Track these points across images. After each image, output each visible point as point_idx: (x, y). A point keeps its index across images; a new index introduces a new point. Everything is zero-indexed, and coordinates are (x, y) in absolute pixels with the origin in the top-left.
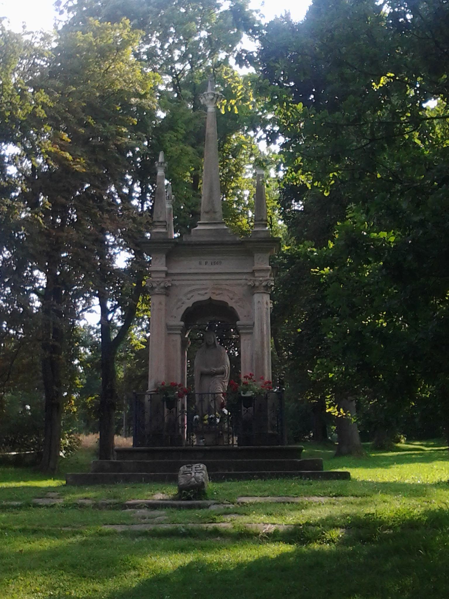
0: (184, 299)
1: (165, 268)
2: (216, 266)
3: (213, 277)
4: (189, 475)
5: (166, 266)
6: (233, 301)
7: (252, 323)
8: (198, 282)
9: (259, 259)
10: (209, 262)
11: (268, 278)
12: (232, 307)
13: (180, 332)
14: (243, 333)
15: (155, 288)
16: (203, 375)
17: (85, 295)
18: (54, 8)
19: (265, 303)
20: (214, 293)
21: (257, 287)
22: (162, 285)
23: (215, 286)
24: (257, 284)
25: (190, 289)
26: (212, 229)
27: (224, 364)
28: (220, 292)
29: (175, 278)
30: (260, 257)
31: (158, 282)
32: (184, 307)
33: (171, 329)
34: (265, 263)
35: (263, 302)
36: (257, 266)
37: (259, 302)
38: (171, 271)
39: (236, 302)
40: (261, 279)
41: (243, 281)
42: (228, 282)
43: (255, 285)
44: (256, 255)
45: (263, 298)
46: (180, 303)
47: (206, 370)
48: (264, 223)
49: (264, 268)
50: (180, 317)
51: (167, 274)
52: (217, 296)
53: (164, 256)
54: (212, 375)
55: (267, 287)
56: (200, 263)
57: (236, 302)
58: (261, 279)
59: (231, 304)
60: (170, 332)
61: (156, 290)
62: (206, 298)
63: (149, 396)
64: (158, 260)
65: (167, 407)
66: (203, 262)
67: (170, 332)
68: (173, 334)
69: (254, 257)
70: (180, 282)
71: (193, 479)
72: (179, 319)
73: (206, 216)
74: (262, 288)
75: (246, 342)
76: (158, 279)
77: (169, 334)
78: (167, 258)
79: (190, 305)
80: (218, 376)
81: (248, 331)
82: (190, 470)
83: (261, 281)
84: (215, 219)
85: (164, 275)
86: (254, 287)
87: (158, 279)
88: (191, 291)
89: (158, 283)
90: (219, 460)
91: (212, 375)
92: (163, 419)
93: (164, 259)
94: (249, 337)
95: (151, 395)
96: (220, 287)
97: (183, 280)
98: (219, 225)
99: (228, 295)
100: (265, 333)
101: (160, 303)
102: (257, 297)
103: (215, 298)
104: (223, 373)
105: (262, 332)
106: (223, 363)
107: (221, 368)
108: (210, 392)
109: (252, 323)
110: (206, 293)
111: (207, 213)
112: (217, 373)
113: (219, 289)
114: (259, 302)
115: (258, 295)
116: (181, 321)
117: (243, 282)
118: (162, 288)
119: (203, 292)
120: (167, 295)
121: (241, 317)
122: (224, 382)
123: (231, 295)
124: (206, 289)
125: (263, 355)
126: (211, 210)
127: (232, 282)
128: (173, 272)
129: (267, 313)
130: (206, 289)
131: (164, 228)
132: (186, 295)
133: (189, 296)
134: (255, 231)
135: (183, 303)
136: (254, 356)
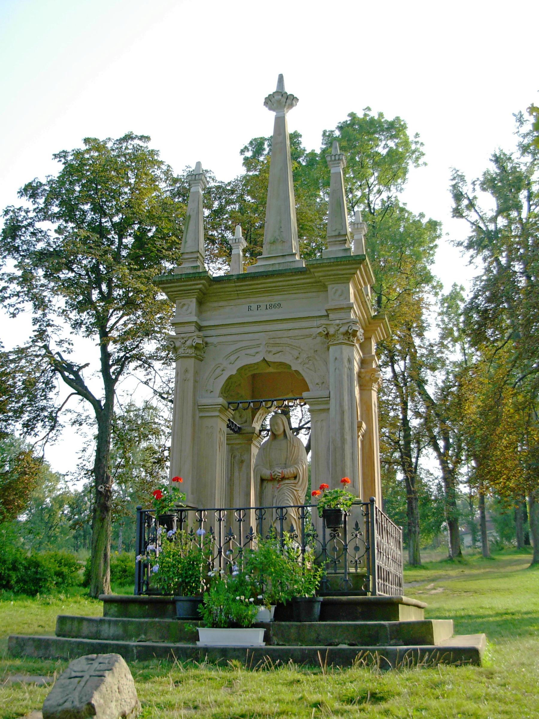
1: (195, 319)
2: (273, 310)
3: (269, 327)
8: (246, 335)
15: (180, 348)
20: (270, 352)
21: (334, 335)
22: (189, 343)
23: (271, 341)
24: (332, 331)
25: (233, 348)
28: (279, 349)
30: (337, 290)
31: (183, 338)
33: (201, 410)
36: (331, 304)
37: (336, 359)
40: (338, 322)
42: (291, 333)
45: (342, 353)
46: (218, 371)
49: (342, 306)
50: (218, 391)
51: (200, 328)
52: (277, 355)
58: (338, 322)
60: (202, 414)
62: (258, 359)
64: (185, 307)
67: (202, 414)
68: (497, 590)
70: (222, 339)
74: (341, 337)
78: (200, 303)
80: (287, 481)
81: (322, 407)
83: (338, 325)
85: (192, 328)
87: (182, 335)
88: (236, 351)
96: (278, 341)
97: (257, 284)
103: (270, 358)
105: (341, 406)
109: (326, 394)
113: (276, 345)
114: (336, 359)
118: (192, 347)
119: (253, 351)
123: (295, 353)
124: (258, 346)
130: (258, 346)
133: (233, 358)
136: (331, 447)
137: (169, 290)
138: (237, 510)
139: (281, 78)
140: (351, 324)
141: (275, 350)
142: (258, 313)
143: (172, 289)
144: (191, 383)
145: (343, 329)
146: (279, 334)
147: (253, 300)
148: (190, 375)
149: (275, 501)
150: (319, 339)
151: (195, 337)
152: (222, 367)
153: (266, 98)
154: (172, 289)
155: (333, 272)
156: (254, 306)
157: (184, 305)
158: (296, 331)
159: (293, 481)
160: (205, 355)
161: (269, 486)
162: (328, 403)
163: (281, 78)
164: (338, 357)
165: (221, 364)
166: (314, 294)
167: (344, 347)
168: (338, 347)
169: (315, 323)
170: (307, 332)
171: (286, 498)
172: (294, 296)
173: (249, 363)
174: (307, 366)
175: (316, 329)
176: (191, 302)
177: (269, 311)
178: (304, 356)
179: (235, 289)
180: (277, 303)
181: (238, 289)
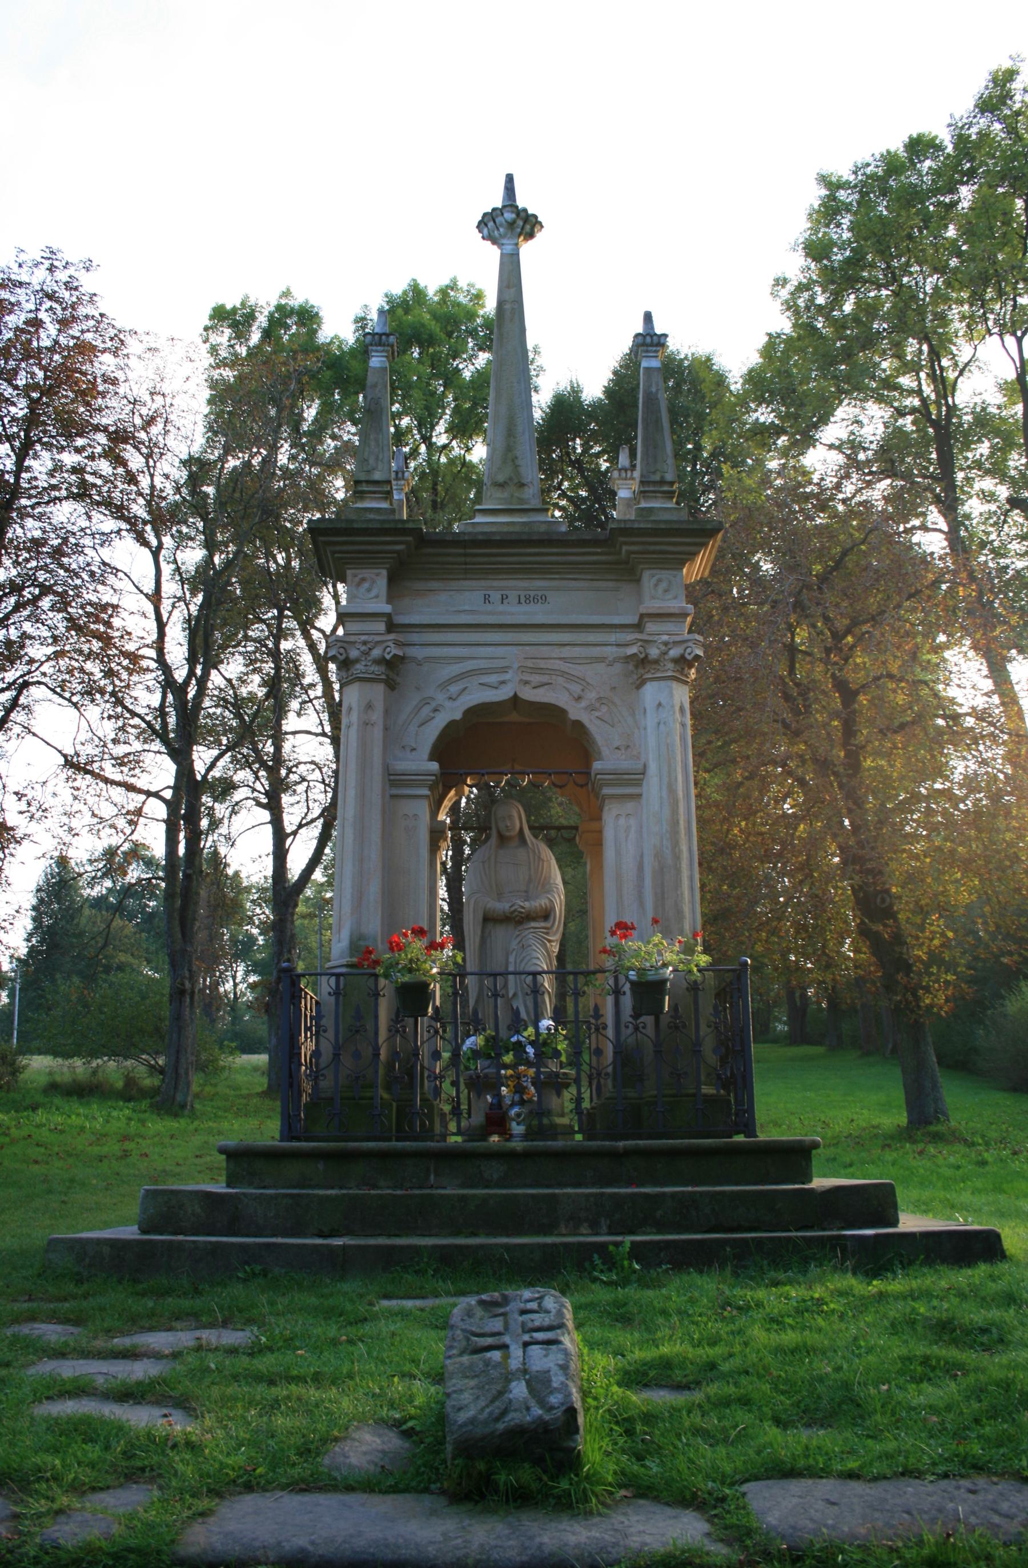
0: (440, 697)
1: (387, 609)
4: (496, 1355)
5: (388, 602)
6: (583, 704)
7: (641, 766)
9: (656, 585)
10: (513, 595)
11: (686, 636)
12: (578, 725)
13: (426, 792)
14: (613, 797)
15: (357, 661)
16: (489, 919)
17: (12, 481)
18: (201, 331)
19: (677, 708)
20: (527, 683)
21: (656, 662)
22: (376, 653)
23: (529, 663)
24: (654, 652)
26: (356, 1141)
27: (549, 891)
28: (545, 679)
29: (415, 638)
30: (660, 580)
31: (365, 643)
32: (440, 721)
33: (393, 784)
34: (675, 598)
35: (673, 706)
37: (660, 705)
38: (399, 619)
39: (591, 708)
41: (609, 649)
42: (566, 652)
43: (646, 656)
44: (646, 575)
46: (426, 711)
47: (502, 906)
48: (666, 488)
49: (672, 611)
51: (392, 627)
52: (541, 691)
53: (384, 572)
54: (518, 919)
55: (683, 662)
56: (487, 599)
57: (591, 708)
58: (665, 638)
59: (576, 712)
60: (395, 791)
61: (360, 666)
62: (503, 694)
63: (333, 980)
64: (366, 585)
65: (474, 517)
66: (495, 596)
67: (395, 791)
69: (638, 581)
71: (519, 1390)
72: (426, 756)
73: (499, 494)
74: (670, 666)
75: (622, 821)
76: (363, 638)
77: (392, 796)
78: (391, 580)
79: (458, 716)
80: (533, 924)
82: (497, 1325)
83: (666, 644)
84: (521, 501)
85: (381, 627)
86: (643, 662)
87: (363, 638)
89: (363, 648)
90: (557, 1191)
91: (518, 919)
92: (377, 1055)
93: (382, 583)
94: (630, 806)
95: (338, 976)
96: (542, 664)
97: (449, 555)
98: (531, 514)
99: (567, 690)
100: (680, 794)
101: (369, 706)
102: (650, 691)
103: (528, 694)
104: (546, 915)
105: (672, 790)
106: (546, 886)
107: (542, 902)
108: (511, 969)
110: (503, 682)
111: (501, 485)
112: (529, 917)
114: (660, 705)
115: (655, 684)
116: (431, 758)
117: (610, 652)
119: (493, 679)
120: (391, 685)
121: (605, 751)
122: (550, 941)
123: (576, 688)
124: (504, 670)
125: (677, 858)
126: (511, 479)
127: (577, 652)
128: (407, 622)
129: (683, 739)
130: (504, 670)
131: (386, 499)
132: (444, 685)
133: (454, 689)
134: (643, 509)
135: (436, 710)
137: (338, 548)
138: (490, 975)
139: (510, 179)
140: (690, 644)
141: (536, 679)
142: (501, 608)
143: (345, 548)
144: (378, 733)
145: (675, 652)
146: (545, 651)
147: (496, 583)
148: (377, 716)
149: (512, 959)
150: (618, 667)
151: (390, 644)
152: (433, 704)
153: (485, 215)
154: (345, 548)
155: (658, 548)
156: (495, 596)
157: (363, 580)
158: (577, 649)
159: (543, 924)
160: (398, 680)
161: (500, 934)
162: (638, 783)
163: (510, 179)
164: (663, 702)
165: (433, 699)
166: (611, 584)
167: (675, 685)
168: (663, 683)
169: (613, 637)
170: (596, 651)
171: (535, 954)
172: (573, 584)
173: (487, 700)
174: (597, 714)
175: (614, 649)
176: (378, 575)
177: (524, 608)
178: (591, 695)
179: (462, 559)
180: (540, 593)
181: (468, 559)
